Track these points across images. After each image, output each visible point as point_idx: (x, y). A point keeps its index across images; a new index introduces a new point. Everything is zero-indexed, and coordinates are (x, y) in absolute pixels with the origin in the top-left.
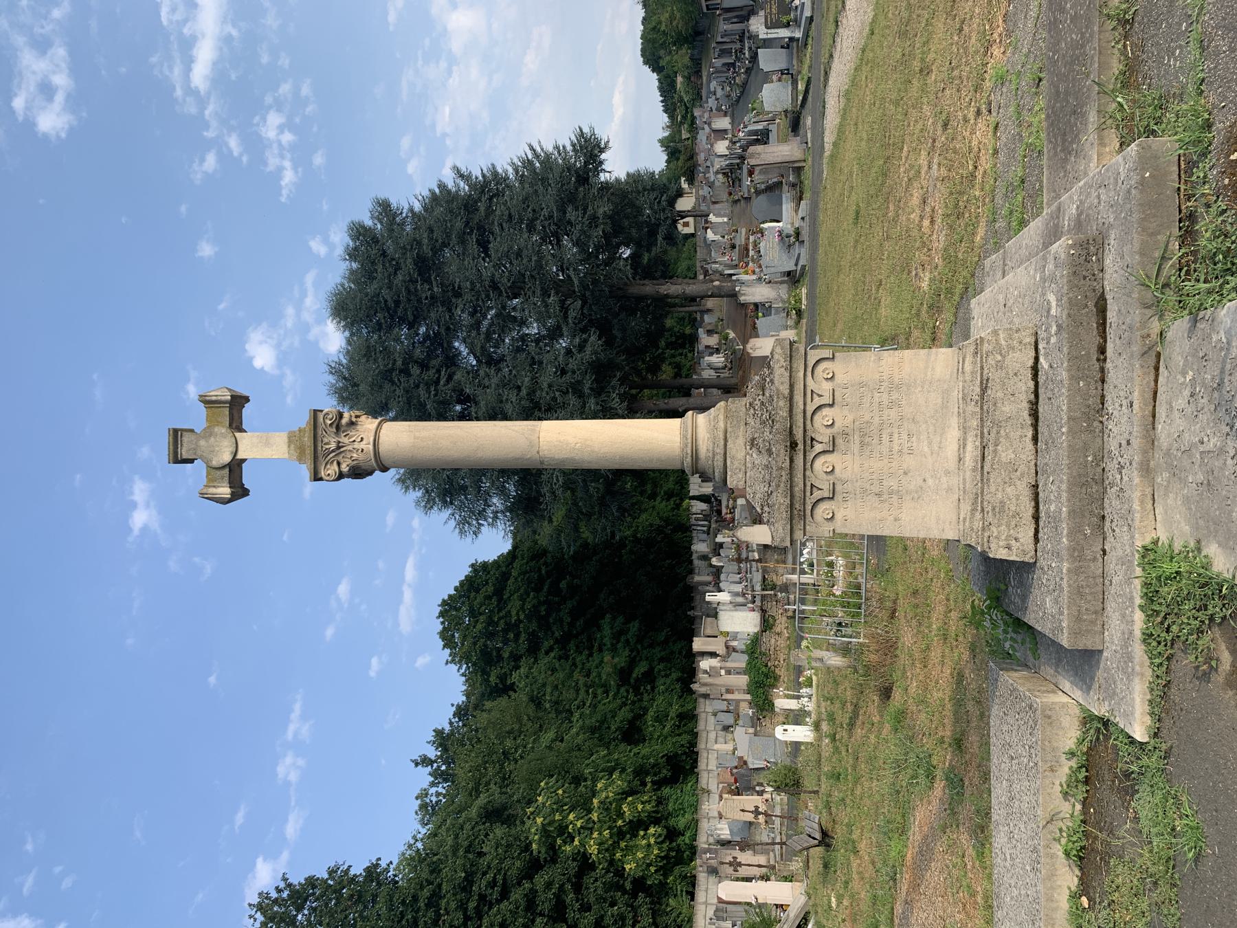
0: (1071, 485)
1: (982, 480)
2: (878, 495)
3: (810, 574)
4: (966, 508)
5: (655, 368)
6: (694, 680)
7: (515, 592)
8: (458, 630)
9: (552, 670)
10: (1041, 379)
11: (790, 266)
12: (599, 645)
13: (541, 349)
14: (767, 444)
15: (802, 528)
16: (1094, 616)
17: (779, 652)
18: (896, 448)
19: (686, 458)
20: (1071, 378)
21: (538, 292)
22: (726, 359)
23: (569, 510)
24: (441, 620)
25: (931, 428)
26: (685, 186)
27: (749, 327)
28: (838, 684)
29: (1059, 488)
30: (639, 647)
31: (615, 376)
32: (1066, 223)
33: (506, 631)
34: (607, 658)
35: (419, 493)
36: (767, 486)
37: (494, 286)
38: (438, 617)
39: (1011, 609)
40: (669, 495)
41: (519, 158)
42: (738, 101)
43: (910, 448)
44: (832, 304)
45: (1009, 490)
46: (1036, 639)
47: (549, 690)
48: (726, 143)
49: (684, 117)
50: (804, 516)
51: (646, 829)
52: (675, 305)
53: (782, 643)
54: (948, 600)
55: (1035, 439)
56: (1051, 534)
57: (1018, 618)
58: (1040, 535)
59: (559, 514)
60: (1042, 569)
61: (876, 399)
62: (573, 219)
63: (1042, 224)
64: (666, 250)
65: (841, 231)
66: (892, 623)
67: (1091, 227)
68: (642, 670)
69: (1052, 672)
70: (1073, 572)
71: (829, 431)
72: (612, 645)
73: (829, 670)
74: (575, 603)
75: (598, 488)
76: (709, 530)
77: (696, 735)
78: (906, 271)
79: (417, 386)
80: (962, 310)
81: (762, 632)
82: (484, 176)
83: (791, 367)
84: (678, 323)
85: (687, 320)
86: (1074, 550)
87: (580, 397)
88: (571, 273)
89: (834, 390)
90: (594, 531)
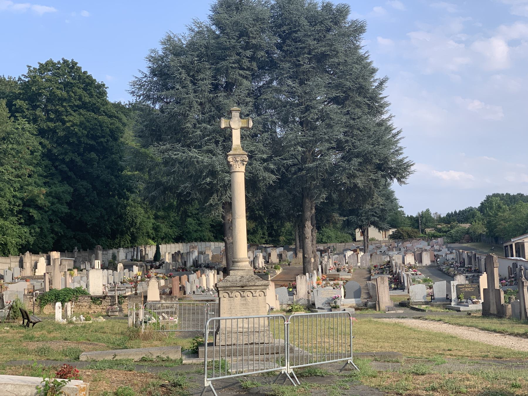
12: (48, 182)
22: (261, 269)
24: (61, 62)
26: (391, 232)
33: (56, 112)
35: (161, 53)
38: (63, 59)
40: (156, 229)
41: (392, 124)
42: (441, 270)
47: (15, 146)
48: (412, 262)
49: (439, 230)
62: (353, 162)
68: (35, 216)
71: (246, 296)
79: (238, 54)
85: (289, 237)
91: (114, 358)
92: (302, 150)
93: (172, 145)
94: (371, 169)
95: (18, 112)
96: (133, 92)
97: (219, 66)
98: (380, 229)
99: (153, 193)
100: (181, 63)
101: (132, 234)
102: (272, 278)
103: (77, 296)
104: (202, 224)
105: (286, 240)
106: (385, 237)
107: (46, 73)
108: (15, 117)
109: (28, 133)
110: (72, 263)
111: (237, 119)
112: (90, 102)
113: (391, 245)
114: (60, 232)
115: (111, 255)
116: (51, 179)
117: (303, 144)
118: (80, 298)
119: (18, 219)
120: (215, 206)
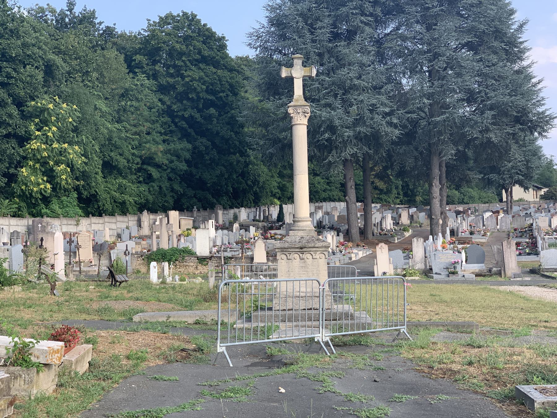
12: (168, 140)
17: (185, 268)
22: (388, 231)
24: (181, 15)
26: (542, 192)
31: (370, 149)
33: (175, 66)
34: (161, 147)
41: (532, 72)
47: (134, 103)
51: (47, 181)
61: (314, 270)
62: (486, 115)
68: (153, 174)
72: (170, 150)
77: (112, 214)
82: (521, 43)
87: (354, 124)
91: (167, 319)
93: (288, 99)
94: (508, 122)
95: (138, 68)
97: (339, 12)
98: (526, 188)
100: (298, 11)
101: (256, 194)
102: (399, 240)
104: (331, 182)
105: (423, 200)
106: (537, 198)
107: (165, 27)
108: (135, 73)
109: (147, 89)
110: (191, 222)
111: (299, 67)
113: (540, 206)
114: (179, 191)
115: (232, 215)
116: (171, 136)
117: (430, 96)
118: (186, 258)
119: (137, 177)
120: (334, 163)
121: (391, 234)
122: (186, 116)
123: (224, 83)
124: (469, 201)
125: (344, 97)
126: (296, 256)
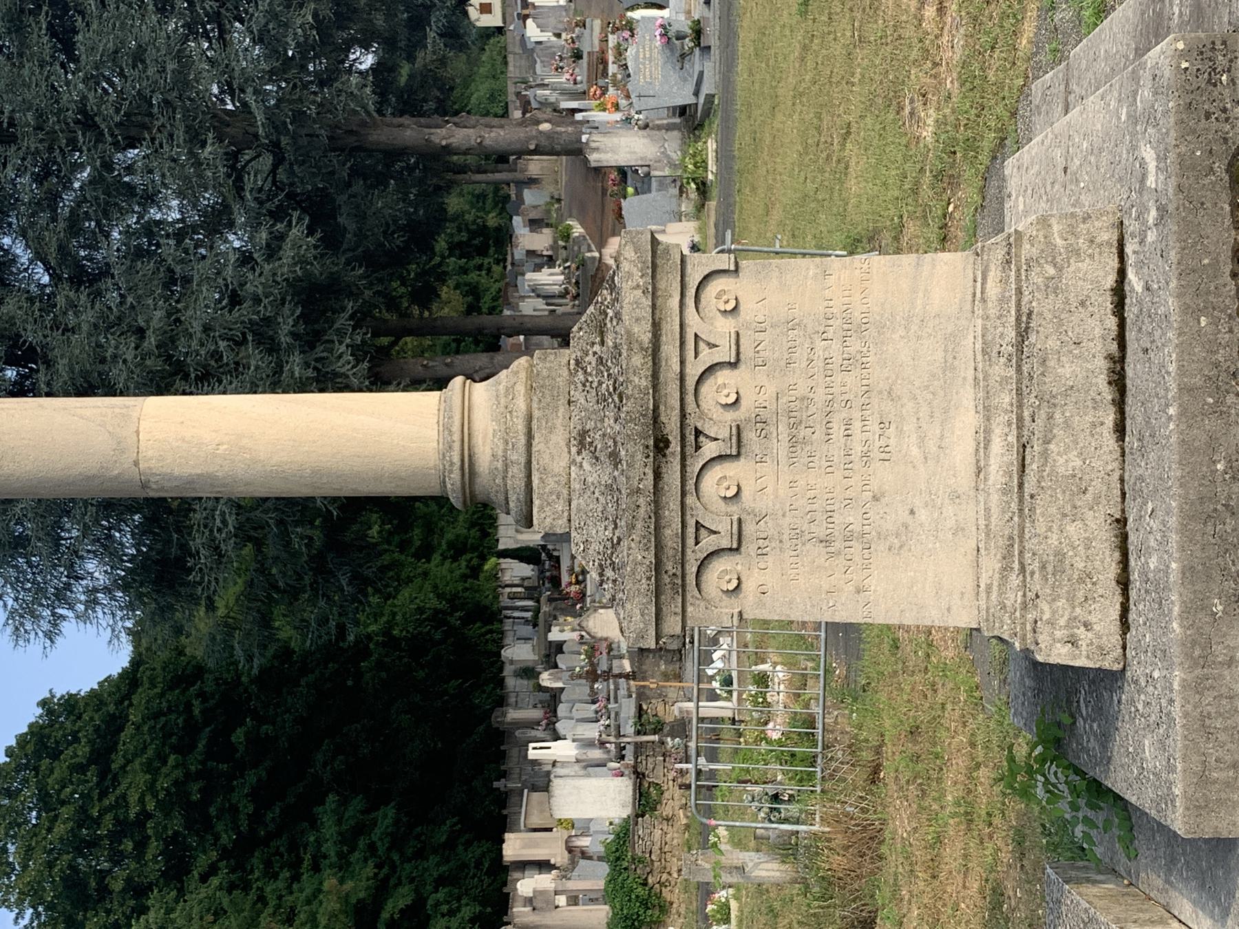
0: (1188, 518)
1: (1021, 510)
2: (826, 541)
3: (726, 699)
4: (991, 565)
5: (425, 295)
6: (505, 919)
7: (135, 755)
8: (13, 837)
9: (216, 914)
10: (1131, 313)
11: (684, 96)
12: (314, 857)
13: (186, 251)
14: (611, 443)
15: (679, 610)
16: (1231, 773)
17: (668, 856)
18: (858, 449)
19: (451, 472)
20: (1185, 309)
21: (180, 135)
22: (568, 278)
23: (250, 584)
25: (924, 411)
27: (610, 217)
28: (776, 916)
29: (1164, 523)
30: (396, 857)
32: (1176, 10)
33: (116, 836)
34: (330, 883)
36: (611, 527)
37: (88, 121)
39: (1083, 761)
40: (458, 549)
43: (885, 449)
44: (763, 171)
45: (1071, 529)
46: (1130, 818)
50: (684, 586)
52: (462, 169)
53: (675, 836)
54: (973, 745)
55: (1120, 430)
56: (1151, 615)
57: (1095, 780)
58: (1132, 616)
59: (229, 595)
60: (1136, 682)
61: (820, 352)
63: (1134, 13)
64: (444, 56)
65: (778, 29)
66: (870, 792)
67: (1220, 17)
68: (401, 904)
69: (1159, 882)
70: (1197, 687)
71: (730, 416)
72: (341, 855)
73: (760, 888)
74: (264, 774)
75: (311, 538)
76: (536, 616)
78: (894, 107)
80: (994, 183)
81: (637, 816)
83: (654, 288)
84: (472, 206)
85: (489, 201)
86: (1194, 643)
87: (270, 351)
88: (250, 98)
89: (738, 334)
90: (303, 626)
92: (213, 144)
93: (198, 531)
96: (50, 636)
99: (344, 583)
102: (593, 247)
103: (634, 859)
110: (535, 795)
112: (89, 741)
116: (305, 849)
121: (578, 268)
122: (251, 809)
123: (164, 704)
124: (500, 102)
125: (193, 376)
126: (714, 484)
